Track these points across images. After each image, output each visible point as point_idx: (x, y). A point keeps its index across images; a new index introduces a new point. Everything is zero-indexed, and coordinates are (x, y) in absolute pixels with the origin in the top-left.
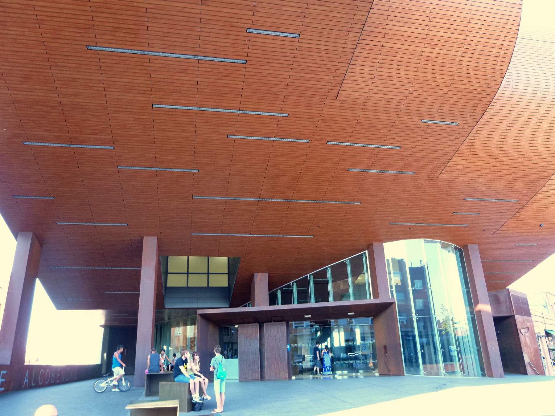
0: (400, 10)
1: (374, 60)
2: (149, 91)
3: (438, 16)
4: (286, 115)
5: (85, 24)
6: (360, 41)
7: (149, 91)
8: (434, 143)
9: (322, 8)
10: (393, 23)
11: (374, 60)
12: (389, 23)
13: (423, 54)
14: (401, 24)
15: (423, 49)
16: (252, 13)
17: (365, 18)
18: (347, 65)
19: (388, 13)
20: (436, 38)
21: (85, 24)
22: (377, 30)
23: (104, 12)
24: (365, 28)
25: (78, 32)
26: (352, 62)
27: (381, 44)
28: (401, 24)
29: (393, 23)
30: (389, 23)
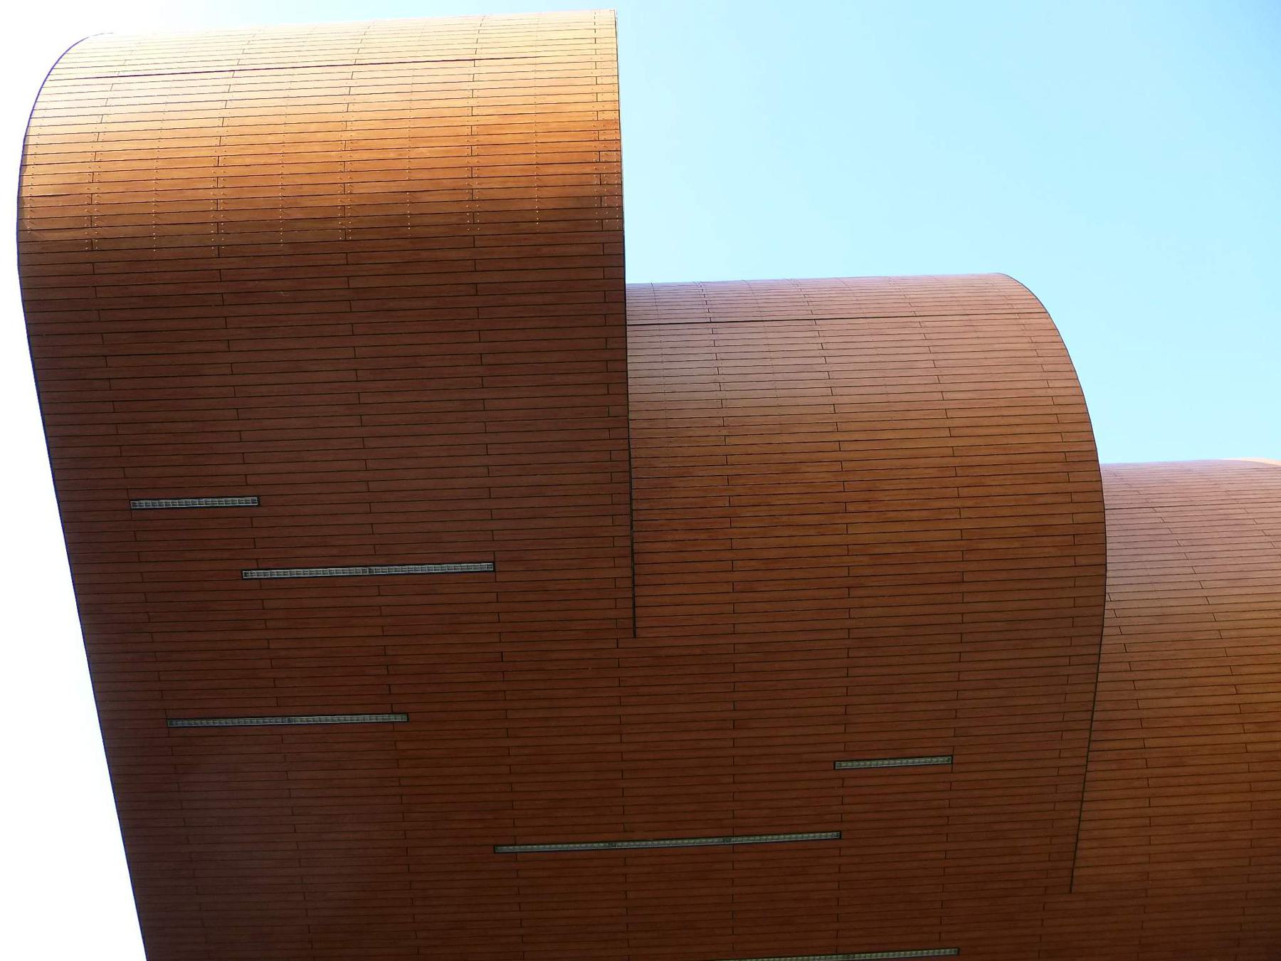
0: (1158, 665)
1: (1137, 784)
2: (623, 932)
3: (1249, 661)
4: (953, 952)
5: (1172, 852)
6: (1093, 746)
7: (623, 932)
8: (1154, 551)
9: (993, 693)
10: (1150, 694)
11: (1137, 784)
12: (1142, 694)
13: (1250, 747)
14: (1171, 693)
15: (1244, 738)
16: (841, 729)
17: (1091, 696)
18: (1077, 805)
19: (1132, 676)
20: (1264, 708)
21: (1172, 852)
22: (1118, 715)
23: (538, 773)
24: (1097, 716)
25: (479, 819)
26: (1087, 796)
27: (1140, 744)
28: (1171, 693)
29: (1150, 694)
30: (1142, 694)
